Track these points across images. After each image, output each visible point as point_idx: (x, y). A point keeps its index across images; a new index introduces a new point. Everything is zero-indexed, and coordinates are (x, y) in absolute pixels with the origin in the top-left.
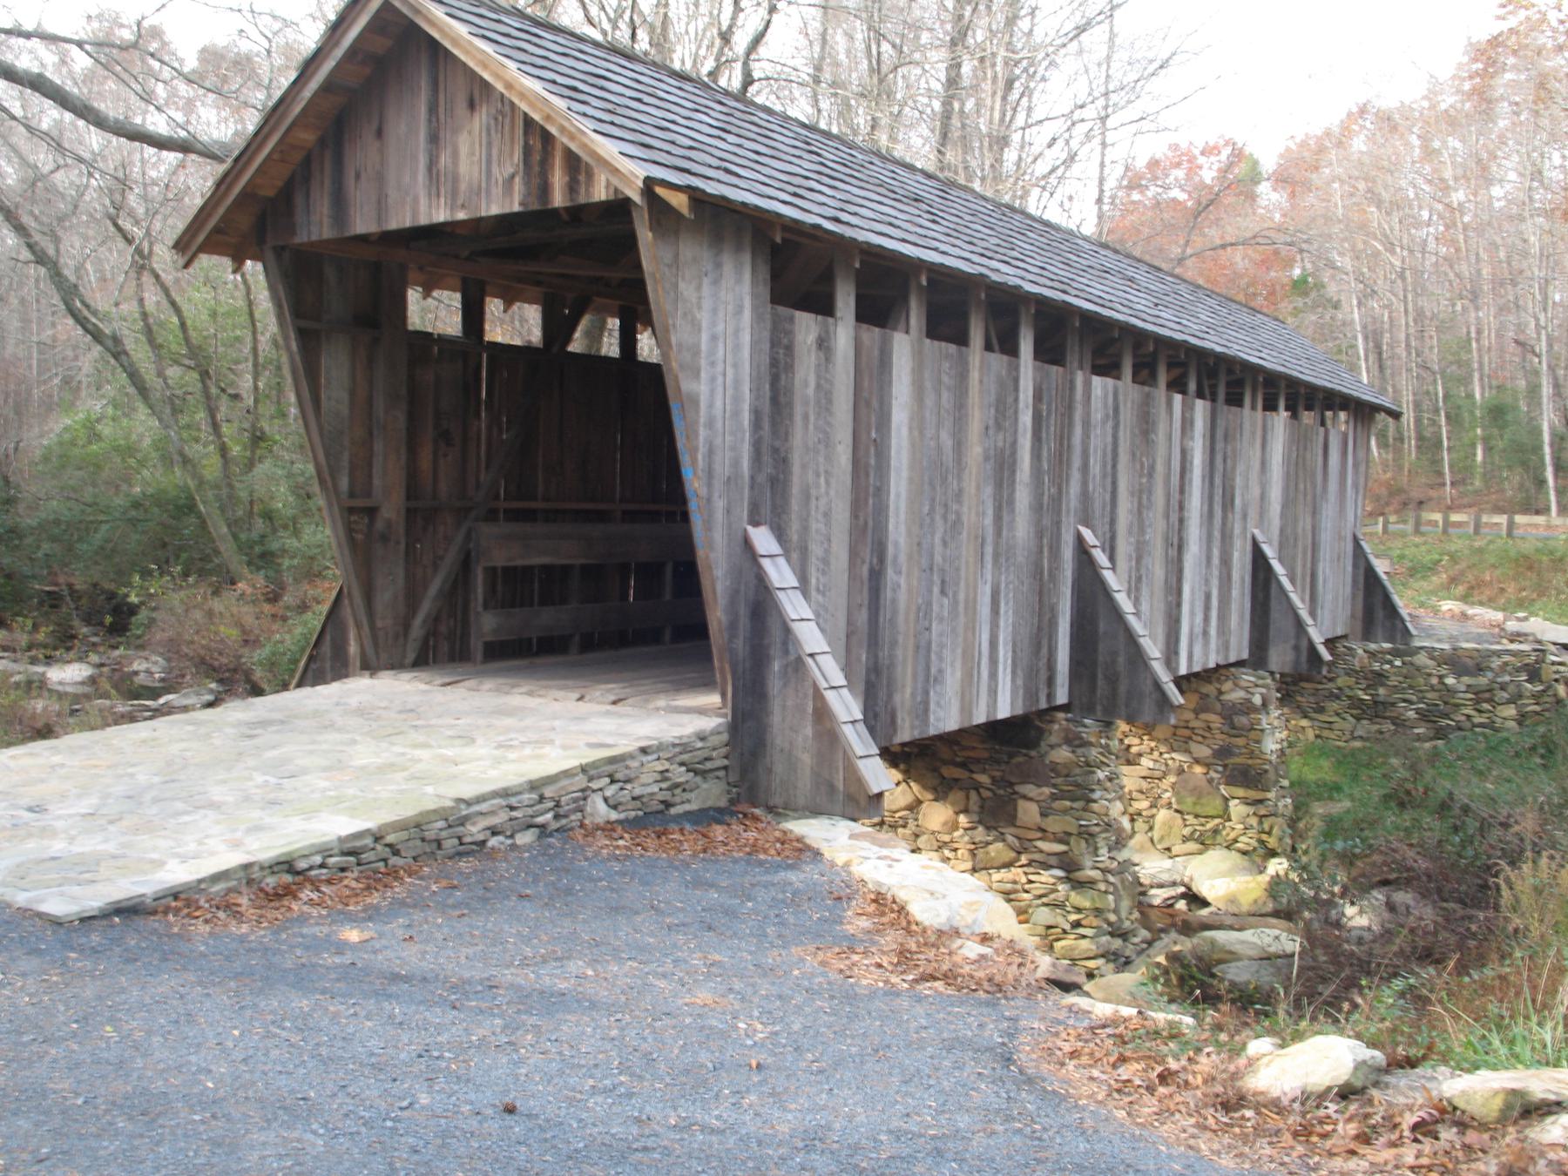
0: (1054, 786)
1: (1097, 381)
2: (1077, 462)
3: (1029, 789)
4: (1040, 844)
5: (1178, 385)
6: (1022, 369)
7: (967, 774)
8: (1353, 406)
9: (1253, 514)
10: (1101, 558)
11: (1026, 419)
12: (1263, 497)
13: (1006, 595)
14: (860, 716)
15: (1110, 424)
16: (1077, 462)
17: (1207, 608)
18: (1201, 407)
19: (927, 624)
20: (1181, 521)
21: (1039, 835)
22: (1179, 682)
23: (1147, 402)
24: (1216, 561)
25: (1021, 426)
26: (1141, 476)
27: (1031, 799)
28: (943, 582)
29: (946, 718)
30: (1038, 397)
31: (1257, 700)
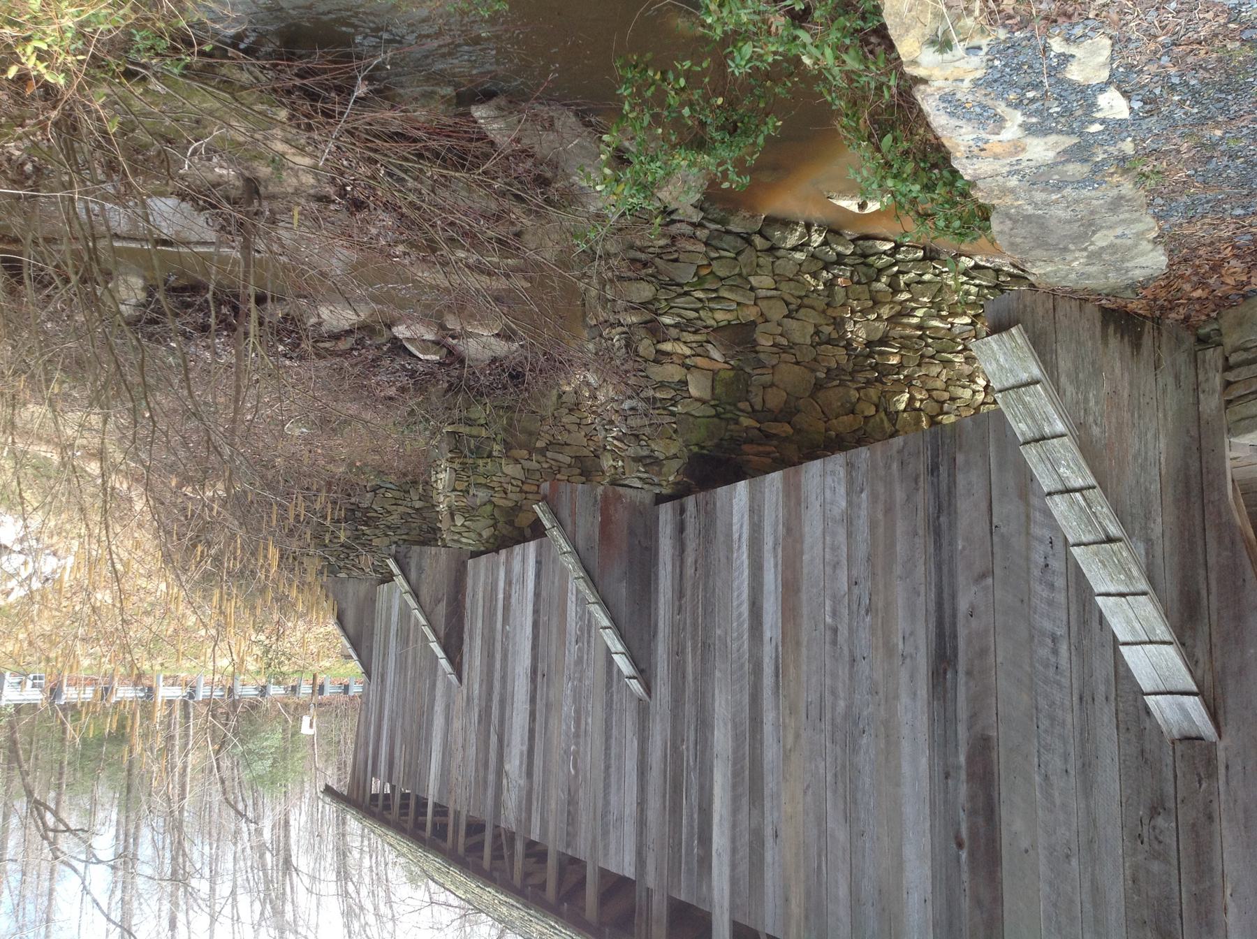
0: (673, 414)
1: (629, 872)
2: (655, 776)
3: (697, 410)
4: (688, 352)
5: (536, 852)
6: (726, 904)
7: (765, 426)
8: (528, 532)
9: (460, 702)
10: (622, 663)
11: (720, 840)
12: (448, 720)
13: (740, 625)
14: (1031, 454)
15: (612, 818)
16: (655, 776)
17: (506, 608)
18: (510, 818)
19: (856, 590)
20: (533, 700)
21: (688, 361)
22: (537, 530)
23: (571, 837)
24: (498, 656)
25: (727, 832)
26: (577, 753)
27: (697, 400)
28: (834, 643)
29: (824, 480)
30: (705, 862)
31: (459, 521)
